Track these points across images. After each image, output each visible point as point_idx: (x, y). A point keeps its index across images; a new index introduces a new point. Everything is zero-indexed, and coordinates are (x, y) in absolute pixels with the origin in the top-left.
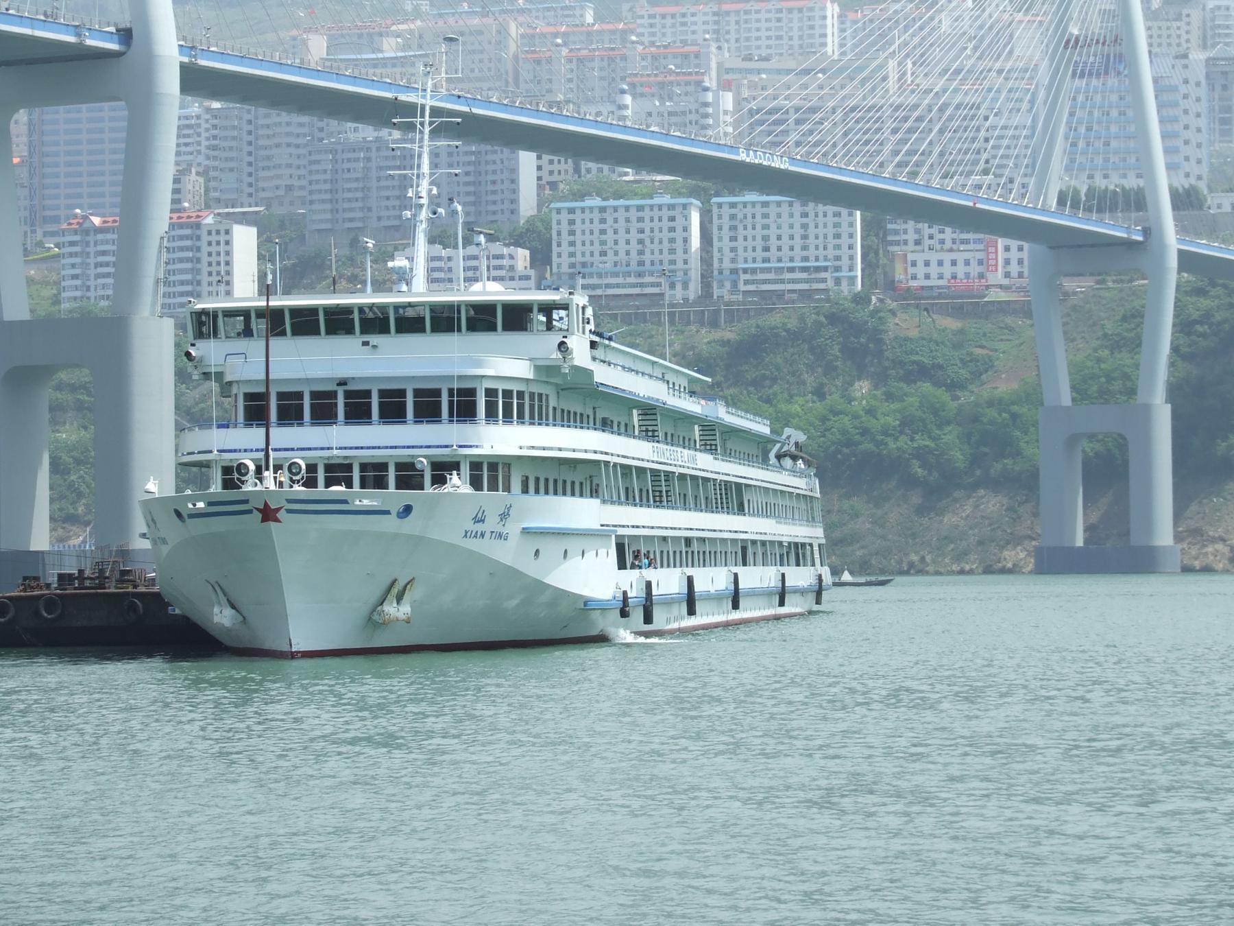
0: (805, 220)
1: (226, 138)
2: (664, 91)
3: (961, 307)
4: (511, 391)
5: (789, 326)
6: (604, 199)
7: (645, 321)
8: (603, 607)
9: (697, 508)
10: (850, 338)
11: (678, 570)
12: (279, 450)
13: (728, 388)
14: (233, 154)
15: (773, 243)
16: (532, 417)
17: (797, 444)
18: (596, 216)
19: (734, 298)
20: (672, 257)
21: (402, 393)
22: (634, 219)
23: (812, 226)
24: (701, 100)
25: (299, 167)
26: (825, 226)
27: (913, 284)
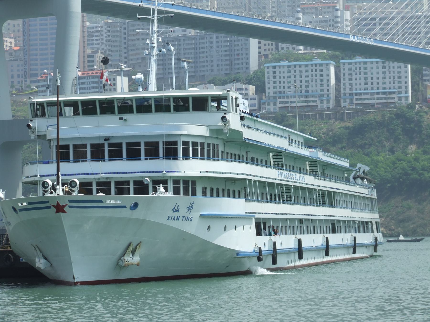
0: (384, 70)
1: (114, 36)
4: (197, 143)
5: (377, 120)
6: (289, 62)
8: (248, 256)
9: (305, 204)
11: (322, 234)
12: (65, 175)
13: (348, 149)
14: (118, 44)
15: (369, 81)
16: (209, 156)
17: (364, 172)
18: (286, 69)
19: (351, 107)
20: (322, 88)
21: (138, 144)
22: (303, 71)
23: (387, 73)
26: (394, 72)
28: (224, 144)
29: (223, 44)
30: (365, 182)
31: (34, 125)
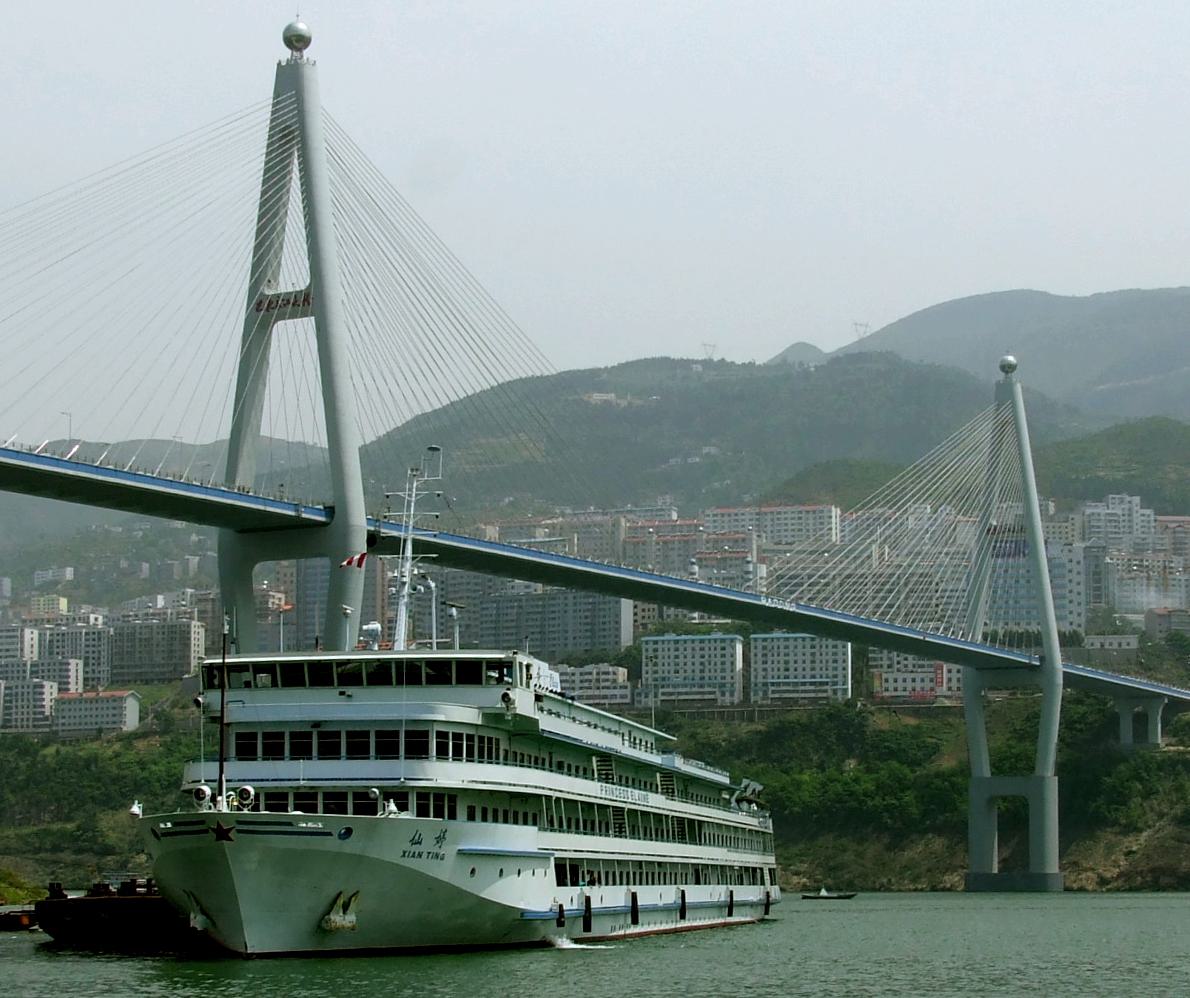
2: (722, 563)
3: (918, 709)
4: (462, 735)
6: (678, 635)
7: (704, 718)
8: (543, 918)
9: (634, 835)
10: (837, 728)
11: (625, 887)
15: (792, 666)
19: (765, 702)
21: (366, 734)
22: (697, 648)
23: (818, 654)
24: (745, 569)
25: (474, 612)
26: (827, 654)
27: (886, 694)
28: (510, 739)
29: (583, 607)
30: (754, 807)
31: (208, 700)
